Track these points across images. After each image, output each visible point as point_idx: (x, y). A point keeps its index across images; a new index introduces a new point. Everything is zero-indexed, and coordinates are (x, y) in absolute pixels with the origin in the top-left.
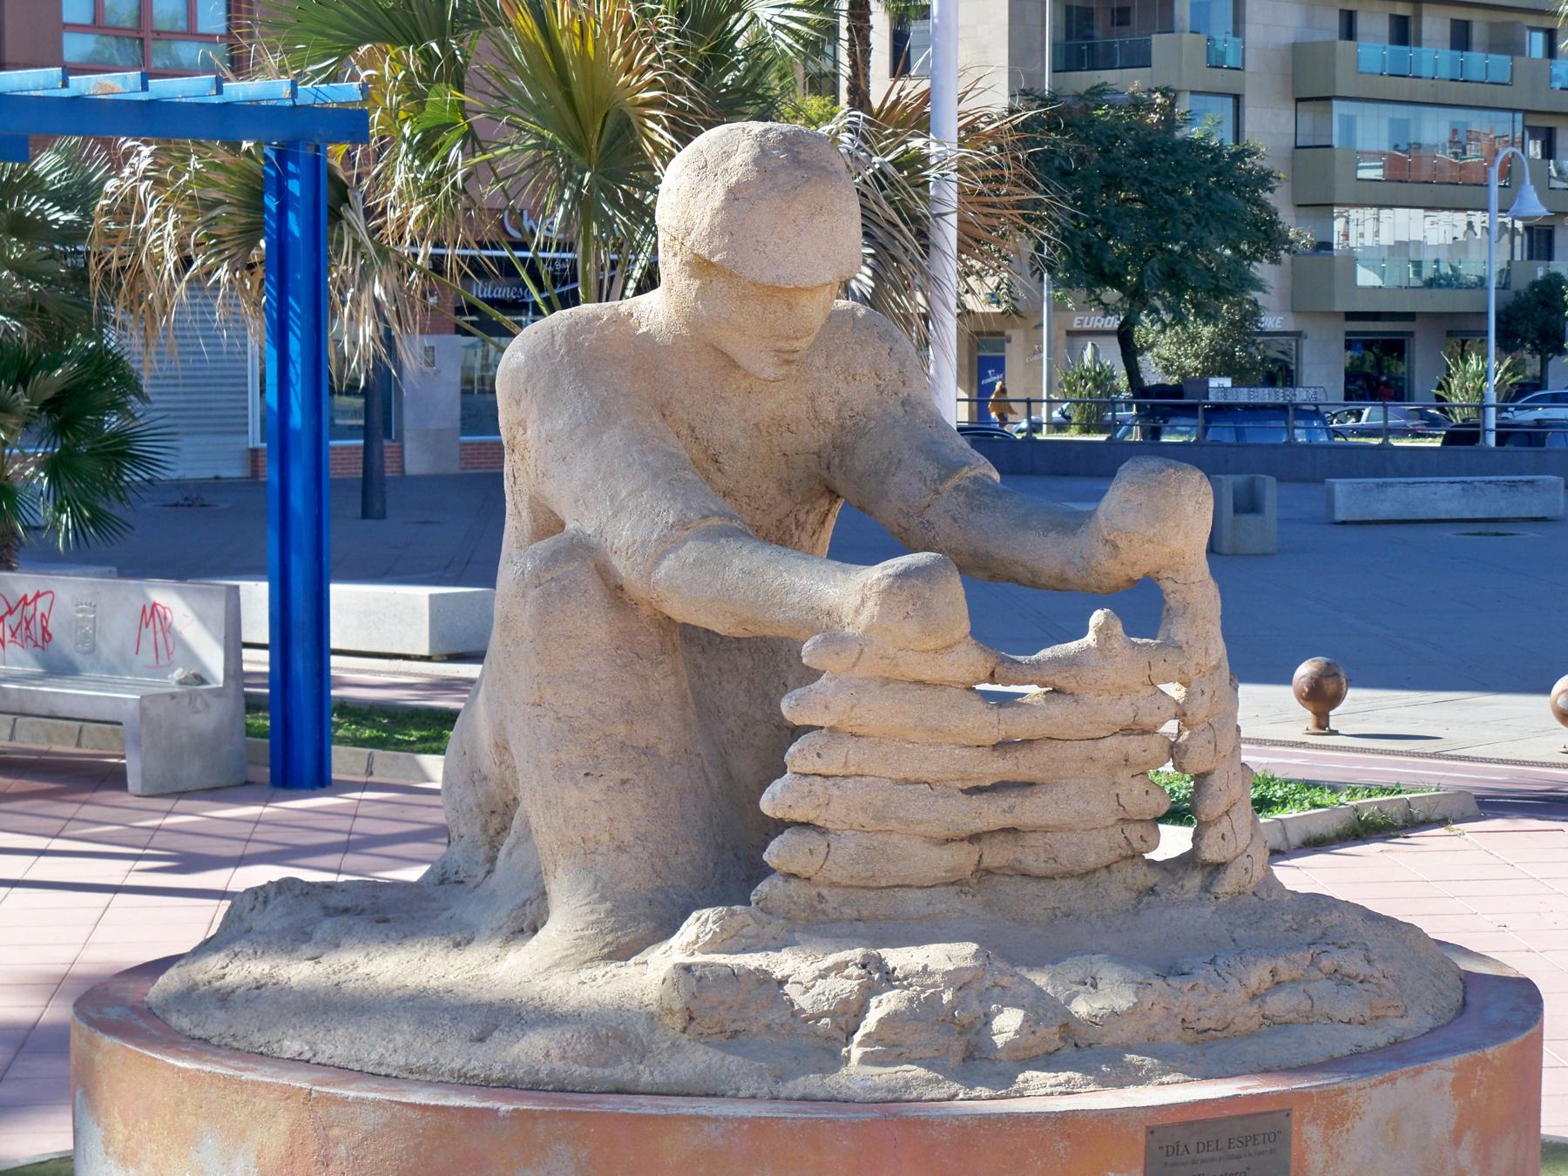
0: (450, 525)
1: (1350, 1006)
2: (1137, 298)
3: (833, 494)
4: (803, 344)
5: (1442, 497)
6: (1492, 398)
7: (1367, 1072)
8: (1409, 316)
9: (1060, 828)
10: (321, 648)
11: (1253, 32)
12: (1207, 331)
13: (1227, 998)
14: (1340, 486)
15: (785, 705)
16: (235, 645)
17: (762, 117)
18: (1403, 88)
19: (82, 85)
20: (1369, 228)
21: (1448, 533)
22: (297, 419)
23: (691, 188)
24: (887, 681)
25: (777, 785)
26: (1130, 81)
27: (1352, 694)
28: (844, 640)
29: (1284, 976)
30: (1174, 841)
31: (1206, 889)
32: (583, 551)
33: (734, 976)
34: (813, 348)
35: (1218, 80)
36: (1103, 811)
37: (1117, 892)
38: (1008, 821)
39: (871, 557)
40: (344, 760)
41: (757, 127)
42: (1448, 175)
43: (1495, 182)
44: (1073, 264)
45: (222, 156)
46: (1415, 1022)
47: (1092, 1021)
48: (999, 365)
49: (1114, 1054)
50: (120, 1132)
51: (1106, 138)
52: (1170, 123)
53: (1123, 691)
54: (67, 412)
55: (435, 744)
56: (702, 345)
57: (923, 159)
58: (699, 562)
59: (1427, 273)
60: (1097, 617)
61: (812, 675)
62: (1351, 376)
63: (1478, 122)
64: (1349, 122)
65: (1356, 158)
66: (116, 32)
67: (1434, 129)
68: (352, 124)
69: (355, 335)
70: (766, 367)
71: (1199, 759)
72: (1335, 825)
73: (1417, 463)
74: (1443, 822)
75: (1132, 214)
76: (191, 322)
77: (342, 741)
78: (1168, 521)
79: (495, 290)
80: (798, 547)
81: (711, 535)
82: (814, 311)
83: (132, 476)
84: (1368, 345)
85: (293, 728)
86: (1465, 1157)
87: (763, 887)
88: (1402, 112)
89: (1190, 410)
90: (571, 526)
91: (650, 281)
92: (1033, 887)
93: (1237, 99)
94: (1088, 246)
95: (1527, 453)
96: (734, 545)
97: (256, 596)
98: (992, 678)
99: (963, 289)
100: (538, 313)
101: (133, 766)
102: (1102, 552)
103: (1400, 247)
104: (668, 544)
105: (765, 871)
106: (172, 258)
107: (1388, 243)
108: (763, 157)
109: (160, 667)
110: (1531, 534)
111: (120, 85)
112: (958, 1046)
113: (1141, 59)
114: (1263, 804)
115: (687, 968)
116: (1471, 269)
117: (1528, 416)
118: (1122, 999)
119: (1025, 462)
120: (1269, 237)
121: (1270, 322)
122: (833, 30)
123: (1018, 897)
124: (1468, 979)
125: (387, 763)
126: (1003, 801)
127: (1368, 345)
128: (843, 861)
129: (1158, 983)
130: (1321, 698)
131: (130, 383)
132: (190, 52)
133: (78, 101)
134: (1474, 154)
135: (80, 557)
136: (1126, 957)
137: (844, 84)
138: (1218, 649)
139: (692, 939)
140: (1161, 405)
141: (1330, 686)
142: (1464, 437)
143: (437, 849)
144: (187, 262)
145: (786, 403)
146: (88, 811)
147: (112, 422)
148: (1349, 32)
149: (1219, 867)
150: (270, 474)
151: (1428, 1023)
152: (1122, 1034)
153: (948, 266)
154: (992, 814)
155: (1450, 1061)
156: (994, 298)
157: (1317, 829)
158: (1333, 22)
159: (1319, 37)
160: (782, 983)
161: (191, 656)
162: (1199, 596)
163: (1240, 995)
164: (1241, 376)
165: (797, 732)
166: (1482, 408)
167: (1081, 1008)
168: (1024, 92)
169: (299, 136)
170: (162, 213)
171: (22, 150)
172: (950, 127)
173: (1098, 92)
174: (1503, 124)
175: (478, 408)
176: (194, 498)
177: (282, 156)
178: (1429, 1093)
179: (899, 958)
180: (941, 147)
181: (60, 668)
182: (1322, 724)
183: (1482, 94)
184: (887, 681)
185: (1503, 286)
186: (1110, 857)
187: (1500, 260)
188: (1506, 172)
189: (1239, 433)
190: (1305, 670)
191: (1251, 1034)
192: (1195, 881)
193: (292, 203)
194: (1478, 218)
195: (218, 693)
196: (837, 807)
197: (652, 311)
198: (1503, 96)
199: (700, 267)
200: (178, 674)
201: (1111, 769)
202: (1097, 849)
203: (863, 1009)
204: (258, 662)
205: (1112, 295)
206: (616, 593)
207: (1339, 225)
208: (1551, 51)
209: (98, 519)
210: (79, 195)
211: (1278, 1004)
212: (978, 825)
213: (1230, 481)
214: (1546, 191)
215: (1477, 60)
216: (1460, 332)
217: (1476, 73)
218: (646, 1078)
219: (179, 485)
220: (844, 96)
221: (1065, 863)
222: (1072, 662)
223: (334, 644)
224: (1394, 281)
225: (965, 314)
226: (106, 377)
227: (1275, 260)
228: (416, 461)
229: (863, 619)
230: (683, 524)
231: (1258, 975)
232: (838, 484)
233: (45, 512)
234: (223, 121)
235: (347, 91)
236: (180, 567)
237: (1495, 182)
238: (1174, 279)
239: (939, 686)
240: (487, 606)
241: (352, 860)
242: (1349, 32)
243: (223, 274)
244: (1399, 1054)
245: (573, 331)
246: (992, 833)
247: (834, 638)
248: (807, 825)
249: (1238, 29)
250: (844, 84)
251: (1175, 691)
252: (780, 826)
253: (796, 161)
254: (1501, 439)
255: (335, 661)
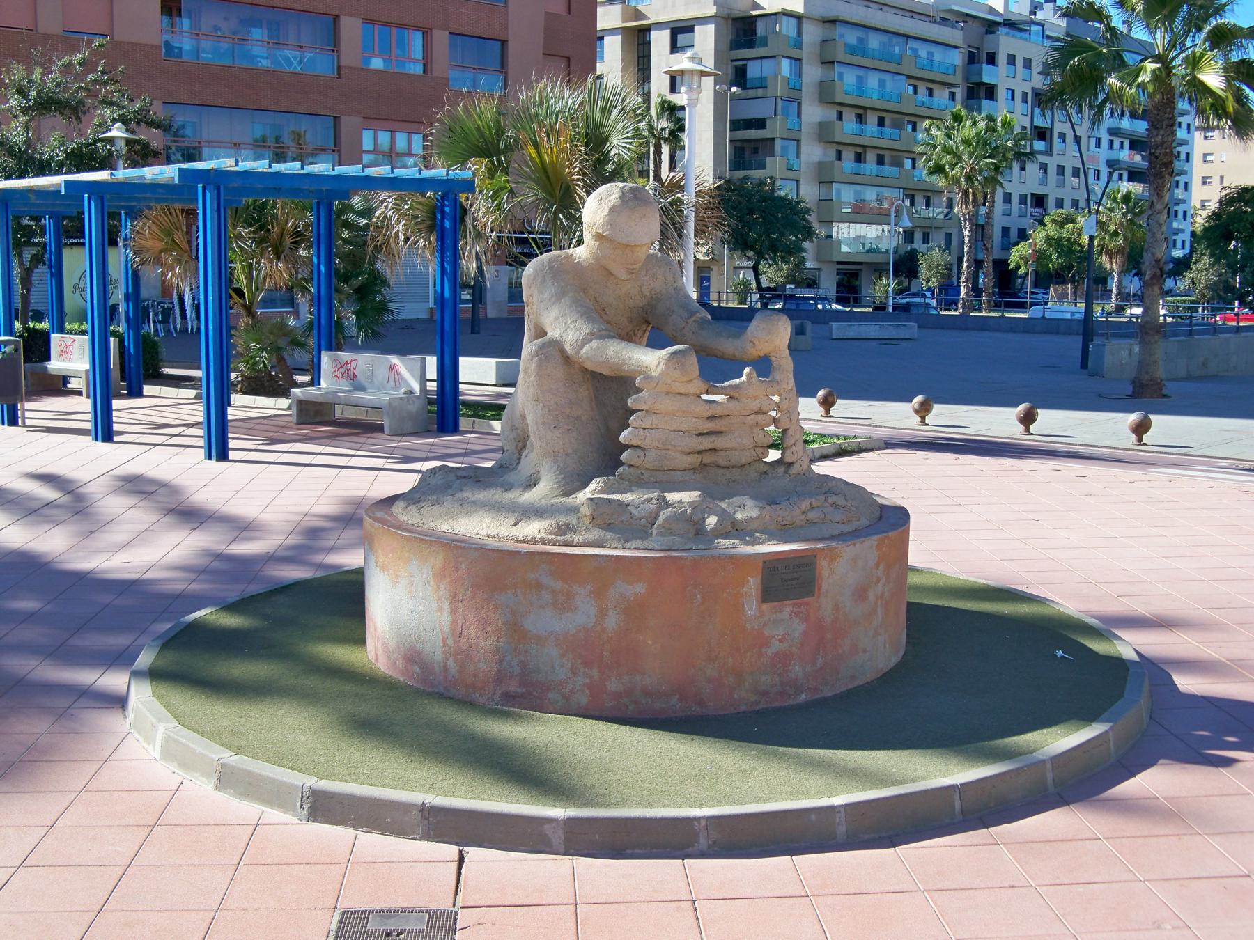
0: (502, 335)
1: (839, 516)
2: (760, 255)
3: (648, 323)
4: (637, 266)
5: (872, 330)
6: (891, 294)
7: (844, 541)
8: (860, 263)
9: (732, 449)
10: (456, 382)
11: (803, 156)
12: (786, 267)
13: (792, 513)
14: (834, 325)
15: (629, 402)
16: (424, 380)
17: (623, 181)
18: (859, 179)
19: (370, 171)
20: (846, 231)
21: (874, 343)
22: (447, 294)
23: (596, 207)
24: (668, 393)
25: (626, 432)
26: (756, 174)
27: (839, 401)
28: (652, 377)
29: (814, 505)
30: (774, 455)
31: (786, 472)
32: (556, 345)
33: (609, 501)
34: (641, 268)
35: (790, 174)
36: (748, 442)
37: (753, 473)
38: (712, 446)
39: (662, 347)
40: (464, 423)
41: (621, 185)
42: (875, 211)
43: (893, 215)
44: (736, 243)
45: (421, 199)
46: (863, 522)
47: (743, 521)
48: (708, 279)
49: (751, 534)
50: (381, 558)
51: (749, 196)
52: (773, 190)
53: (756, 398)
54: (363, 293)
55: (498, 417)
56: (600, 268)
57: (681, 202)
58: (597, 348)
59: (867, 247)
60: (747, 370)
61: (639, 390)
62: (839, 285)
63: (887, 192)
64: (839, 191)
65: (841, 204)
66: (383, 153)
67: (870, 194)
68: (469, 186)
69: (469, 266)
70: (623, 275)
71: (785, 423)
72: (832, 450)
73: (863, 317)
74: (872, 450)
75: (758, 224)
76: (411, 264)
77: (464, 415)
78: (774, 335)
79: (521, 247)
80: (634, 342)
81: (602, 338)
82: (641, 254)
83: (388, 317)
84: (845, 274)
85: (445, 410)
86: (880, 573)
87: (620, 470)
88: (858, 187)
89: (779, 297)
90: (549, 334)
91: (580, 242)
92: (722, 471)
93: (798, 182)
94: (742, 235)
95: (904, 315)
96: (611, 341)
97: (432, 362)
98: (707, 393)
99: (695, 250)
100: (537, 255)
101: (386, 423)
102: (749, 346)
103: (857, 238)
104: (586, 341)
105: (621, 464)
106: (402, 237)
107: (853, 236)
108: (623, 196)
109: (396, 387)
110: (905, 344)
111: (383, 171)
112: (693, 531)
113: (762, 166)
114: (806, 442)
115: (592, 499)
116: (883, 246)
117: (905, 301)
118: (755, 514)
119: (721, 315)
120: (809, 233)
121: (809, 265)
122: (648, 153)
123: (715, 472)
124: (883, 507)
125: (480, 424)
126: (710, 439)
127: (845, 274)
128: (651, 459)
129: (768, 507)
130: (827, 404)
131: (385, 283)
132: (411, 161)
133: (367, 177)
134: (885, 205)
135: (366, 347)
136: (755, 497)
137: (652, 174)
138: (792, 383)
139: (593, 488)
140: (773, 293)
141: (830, 399)
142: (880, 308)
143: (498, 456)
144: (407, 239)
145: (630, 290)
146: (370, 441)
147: (378, 298)
148: (839, 157)
149: (791, 464)
150: (438, 316)
151: (868, 523)
152: (755, 526)
153: (691, 239)
154: (706, 443)
155: (875, 537)
156: (706, 254)
157: (825, 452)
158: (834, 154)
159: (828, 159)
160: (627, 505)
161: (408, 385)
162: (785, 363)
163: (798, 512)
164: (798, 284)
165: (633, 412)
166: (887, 298)
167: (739, 516)
168: (718, 176)
169: (450, 191)
170: (398, 221)
171: (347, 195)
172: (692, 189)
173: (746, 178)
174: (896, 193)
175: (515, 293)
176: (409, 326)
177: (442, 198)
178: (867, 549)
179: (670, 496)
180: (689, 198)
181: (359, 388)
182: (827, 413)
183: (889, 182)
184: (668, 393)
185: (895, 253)
186: (750, 460)
187: (894, 244)
188: (897, 211)
189: (797, 305)
190: (821, 393)
191: (802, 527)
192: (782, 469)
193: (445, 217)
194: (886, 228)
195: (418, 397)
196: (649, 440)
197: (581, 253)
198: (896, 183)
199: (599, 237)
200: (403, 390)
201: (751, 427)
202: (745, 458)
203: (657, 516)
204: (432, 386)
205: (750, 253)
206: (566, 358)
207: (835, 229)
208: (914, 167)
209: (374, 333)
210: (368, 213)
211: (812, 515)
212: (702, 448)
213: (798, 322)
214: (912, 218)
215: (886, 169)
216: (879, 269)
217: (886, 174)
218: (576, 540)
219: (404, 321)
220: (651, 178)
221: (733, 462)
222: (737, 387)
223: (461, 380)
224: (855, 250)
225: (696, 259)
226: (376, 281)
227: (811, 241)
228: (491, 313)
229: (659, 369)
230: (591, 334)
231: (805, 505)
232: (650, 319)
233: (354, 331)
234: (419, 185)
235: (467, 174)
236: (402, 351)
237: (893, 215)
238: (774, 248)
239: (688, 395)
240: (518, 365)
241: (467, 459)
242: (839, 157)
243: (421, 242)
244: (856, 534)
245: (551, 260)
246: (706, 451)
247: (648, 378)
248: (637, 447)
249: (798, 156)
250: (652, 174)
251: (776, 398)
252: (627, 447)
253: (635, 197)
254: (894, 309)
255: (461, 386)
